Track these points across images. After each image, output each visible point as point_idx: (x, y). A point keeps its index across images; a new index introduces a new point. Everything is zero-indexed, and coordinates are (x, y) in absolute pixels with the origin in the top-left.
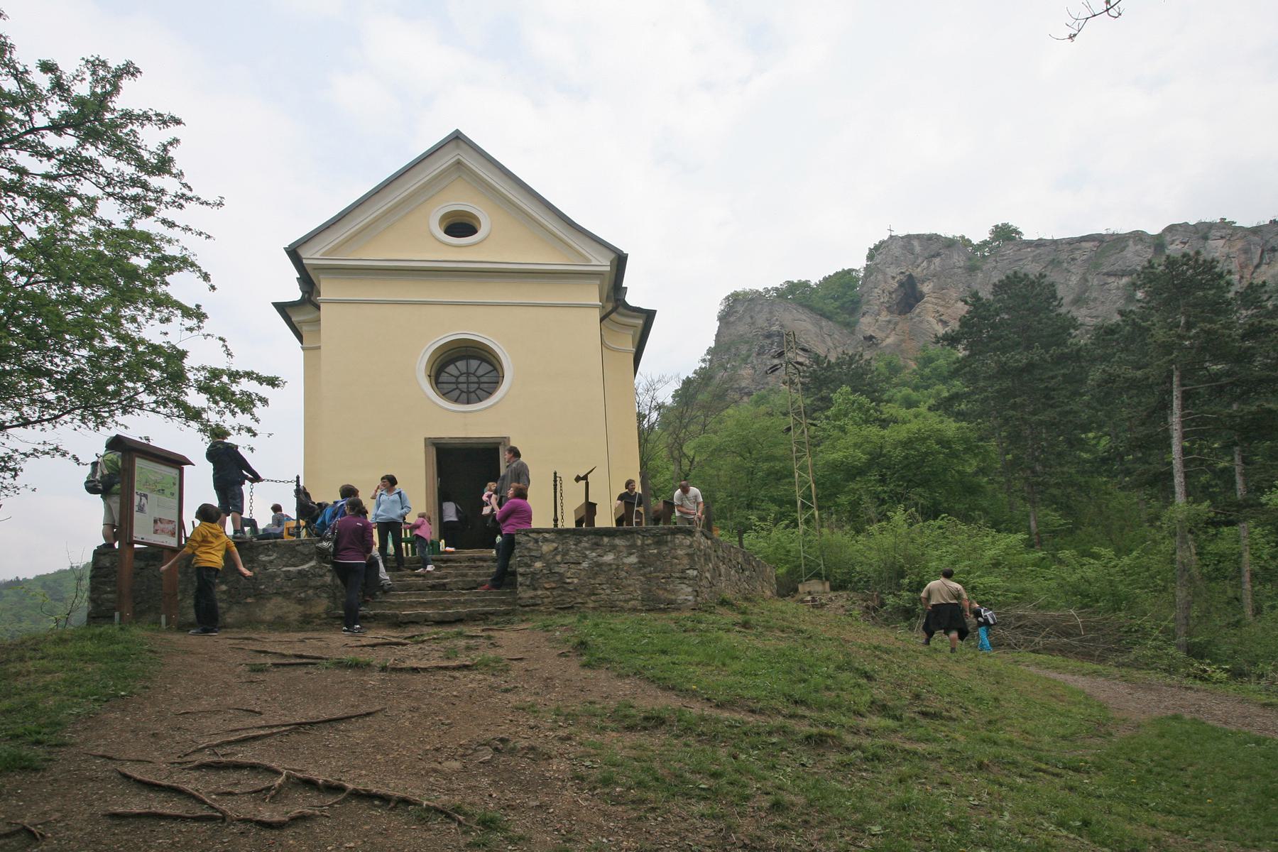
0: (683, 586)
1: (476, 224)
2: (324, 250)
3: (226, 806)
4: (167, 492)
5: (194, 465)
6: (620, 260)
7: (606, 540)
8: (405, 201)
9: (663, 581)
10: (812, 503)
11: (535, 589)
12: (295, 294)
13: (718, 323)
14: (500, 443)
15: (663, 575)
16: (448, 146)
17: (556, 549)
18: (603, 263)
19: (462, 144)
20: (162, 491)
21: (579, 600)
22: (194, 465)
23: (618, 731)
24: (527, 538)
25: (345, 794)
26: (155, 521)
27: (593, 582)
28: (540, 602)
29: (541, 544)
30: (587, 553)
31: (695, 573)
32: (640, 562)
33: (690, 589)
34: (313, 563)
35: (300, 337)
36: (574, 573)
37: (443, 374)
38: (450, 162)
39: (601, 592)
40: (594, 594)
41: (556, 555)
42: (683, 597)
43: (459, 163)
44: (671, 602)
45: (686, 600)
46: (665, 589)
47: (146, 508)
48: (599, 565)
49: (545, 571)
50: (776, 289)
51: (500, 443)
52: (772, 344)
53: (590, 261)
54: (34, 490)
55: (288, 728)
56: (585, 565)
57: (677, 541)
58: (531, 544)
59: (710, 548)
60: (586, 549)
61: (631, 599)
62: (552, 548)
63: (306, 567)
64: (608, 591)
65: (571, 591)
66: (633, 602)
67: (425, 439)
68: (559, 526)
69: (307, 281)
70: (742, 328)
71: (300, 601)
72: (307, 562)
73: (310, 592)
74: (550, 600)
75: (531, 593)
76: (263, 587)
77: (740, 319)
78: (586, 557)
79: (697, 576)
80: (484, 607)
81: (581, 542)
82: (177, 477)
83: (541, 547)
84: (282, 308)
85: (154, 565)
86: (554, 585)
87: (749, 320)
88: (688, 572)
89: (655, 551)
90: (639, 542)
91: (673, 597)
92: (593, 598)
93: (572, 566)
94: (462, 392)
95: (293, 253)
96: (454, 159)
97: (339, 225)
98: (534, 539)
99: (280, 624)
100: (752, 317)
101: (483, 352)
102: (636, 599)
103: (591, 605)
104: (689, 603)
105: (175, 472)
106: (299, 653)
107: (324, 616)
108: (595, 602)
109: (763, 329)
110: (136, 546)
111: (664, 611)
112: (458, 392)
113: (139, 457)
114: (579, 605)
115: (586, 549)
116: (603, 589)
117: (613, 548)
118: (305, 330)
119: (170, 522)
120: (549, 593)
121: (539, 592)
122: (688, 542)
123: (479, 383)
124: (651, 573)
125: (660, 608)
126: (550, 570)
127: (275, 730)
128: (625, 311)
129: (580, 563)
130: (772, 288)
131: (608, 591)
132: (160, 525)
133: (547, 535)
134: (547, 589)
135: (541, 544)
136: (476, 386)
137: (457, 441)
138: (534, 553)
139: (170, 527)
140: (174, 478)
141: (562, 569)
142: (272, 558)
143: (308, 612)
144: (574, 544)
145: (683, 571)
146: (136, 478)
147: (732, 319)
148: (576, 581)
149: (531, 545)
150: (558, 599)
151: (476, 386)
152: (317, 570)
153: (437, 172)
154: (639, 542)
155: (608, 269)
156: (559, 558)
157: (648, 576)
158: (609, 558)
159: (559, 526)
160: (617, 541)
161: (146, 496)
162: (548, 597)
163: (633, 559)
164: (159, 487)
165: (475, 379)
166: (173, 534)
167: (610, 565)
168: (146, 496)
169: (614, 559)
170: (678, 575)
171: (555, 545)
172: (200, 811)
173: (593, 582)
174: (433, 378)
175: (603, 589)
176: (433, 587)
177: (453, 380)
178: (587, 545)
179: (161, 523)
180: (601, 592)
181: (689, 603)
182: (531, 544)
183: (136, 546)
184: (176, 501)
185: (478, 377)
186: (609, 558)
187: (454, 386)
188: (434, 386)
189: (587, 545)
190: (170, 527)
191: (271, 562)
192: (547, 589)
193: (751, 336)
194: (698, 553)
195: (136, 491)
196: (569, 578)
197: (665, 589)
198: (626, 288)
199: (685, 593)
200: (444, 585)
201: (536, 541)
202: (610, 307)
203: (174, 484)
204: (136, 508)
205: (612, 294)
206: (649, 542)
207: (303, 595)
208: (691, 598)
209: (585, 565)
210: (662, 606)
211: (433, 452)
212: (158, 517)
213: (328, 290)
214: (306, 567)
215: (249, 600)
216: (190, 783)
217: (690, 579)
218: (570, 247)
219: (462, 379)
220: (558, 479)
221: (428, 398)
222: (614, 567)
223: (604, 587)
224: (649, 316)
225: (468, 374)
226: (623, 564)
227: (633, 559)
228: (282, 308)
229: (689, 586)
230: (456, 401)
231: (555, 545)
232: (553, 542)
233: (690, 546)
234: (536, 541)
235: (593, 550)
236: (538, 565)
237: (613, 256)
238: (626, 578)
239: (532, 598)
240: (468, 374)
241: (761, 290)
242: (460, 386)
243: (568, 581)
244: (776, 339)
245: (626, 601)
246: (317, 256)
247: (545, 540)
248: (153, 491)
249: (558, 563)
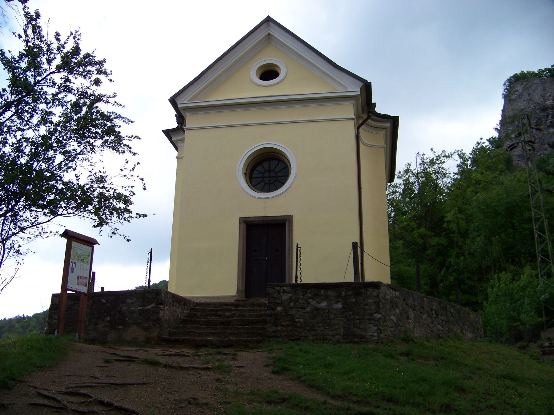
0: (371, 325)
1: (279, 71)
2: (189, 98)
3: (68, 405)
4: (85, 260)
5: (99, 244)
6: (367, 87)
7: (322, 292)
8: (241, 58)
9: (358, 321)
10: (549, 260)
11: (277, 326)
12: (174, 125)
13: (502, 101)
14: (286, 220)
15: (358, 317)
16: (262, 25)
17: (291, 298)
18: (355, 89)
19: (271, 24)
20: (83, 260)
21: (303, 334)
22: (99, 244)
23: (260, 402)
24: (274, 290)
25: (112, 408)
26: (78, 278)
27: (312, 321)
28: (279, 335)
29: (281, 294)
30: (310, 301)
31: (380, 316)
32: (343, 308)
33: (375, 328)
34: (153, 305)
35: (176, 148)
36: (301, 315)
37: (255, 172)
38: (264, 35)
39: (317, 328)
40: (313, 330)
41: (290, 302)
42: (370, 334)
43: (269, 35)
44: (362, 337)
45: (372, 335)
46: (359, 328)
47: (75, 270)
48: (317, 309)
49: (283, 314)
50: (549, 70)
51: (286, 220)
52: (548, 116)
53: (347, 88)
54: (35, 252)
55: (106, 385)
56: (308, 309)
57: (368, 293)
58: (276, 294)
59: (399, 298)
60: (309, 298)
61: (336, 335)
62: (288, 298)
63: (149, 307)
64: (322, 328)
65: (298, 327)
66: (337, 337)
67: (240, 218)
68: (299, 282)
69: (180, 118)
70: (522, 104)
71: (146, 329)
72: (151, 304)
73: (151, 323)
74: (285, 333)
75: (274, 329)
76: (127, 319)
77: (520, 96)
78: (309, 303)
79: (380, 318)
80: (248, 337)
81: (306, 293)
82: (91, 251)
83: (282, 296)
84: (168, 133)
85: (78, 304)
86: (288, 323)
87: (527, 97)
88: (374, 315)
89: (354, 300)
90: (344, 294)
91: (364, 333)
92: (312, 333)
93: (300, 310)
94: (266, 183)
95: (173, 101)
96: (267, 33)
97: (198, 81)
98: (278, 291)
99: (133, 342)
100: (529, 95)
101: (278, 155)
102: (340, 335)
103: (311, 338)
104: (375, 338)
105: (91, 248)
106: (129, 355)
107: (156, 339)
108: (313, 335)
109: (539, 104)
110: (69, 292)
111: (358, 343)
112: (263, 184)
113: (74, 241)
114: (303, 338)
115: (309, 298)
116: (319, 327)
117: (327, 297)
118: (179, 145)
119: (85, 278)
120: (285, 329)
121: (279, 328)
122: (375, 293)
123: (263, 177)
124: (350, 316)
125: (355, 342)
126: (286, 313)
127: (100, 385)
128: (374, 117)
129: (305, 308)
130: (545, 69)
131: (322, 328)
132: (80, 280)
133: (285, 288)
134: (284, 326)
135: (281, 294)
136: (265, 175)
137: (269, 219)
138: (277, 301)
139: (85, 281)
140: (89, 252)
141: (293, 312)
142: (133, 301)
143: (149, 336)
144: (302, 295)
145: (372, 314)
146: (72, 253)
147: (513, 97)
148: (302, 320)
149: (276, 295)
150: (290, 333)
151: (265, 175)
152: (155, 309)
153: (255, 42)
154: (344, 294)
155: (359, 93)
156: (292, 304)
157: (349, 317)
158: (324, 304)
159: (299, 282)
160: (330, 293)
161: (75, 263)
162: (284, 332)
163: (339, 306)
164: (82, 258)
165: (274, 174)
166: (86, 286)
167: (324, 309)
168: (75, 263)
169: (327, 305)
170: (368, 317)
171: (290, 295)
172: (60, 405)
173: (312, 321)
174: (248, 175)
175: (319, 327)
176: (222, 323)
177: (261, 175)
178: (310, 295)
179: (81, 279)
180: (317, 328)
181: (375, 338)
182: (276, 294)
183: (69, 292)
184: (89, 266)
185: (276, 173)
186: (324, 304)
187: (279, 174)
188: (248, 181)
189: (310, 295)
190: (85, 281)
191: (132, 303)
192: (284, 326)
193: (529, 110)
194: (384, 301)
195: (71, 260)
196: (298, 318)
197: (359, 328)
198: (375, 103)
199: (372, 330)
200: (229, 322)
201: (279, 292)
202: (365, 116)
203: (89, 256)
204: (70, 270)
205: (366, 108)
206: (350, 293)
207: (147, 325)
208: (376, 334)
209: (308, 309)
210: (356, 340)
211: (244, 226)
212: (80, 275)
213: (189, 124)
214: (149, 307)
215: (120, 327)
216: (59, 397)
217: (375, 321)
218: (335, 80)
219: (266, 175)
220: (299, 249)
221: (243, 190)
222: (327, 311)
223: (320, 325)
224: (394, 121)
225: (270, 171)
226: (332, 309)
227: (339, 306)
228: (168, 133)
229: (375, 325)
230: (277, 189)
231: (290, 295)
232: (289, 293)
233: (377, 296)
234: (279, 292)
235: (313, 299)
236: (279, 309)
237: (361, 84)
238: (334, 319)
239: (275, 332)
240: (270, 171)
241: (536, 72)
242: (265, 179)
243: (297, 320)
244: (550, 111)
245: (333, 336)
246: (185, 102)
247: (285, 292)
248: (79, 260)
249: (292, 308)
